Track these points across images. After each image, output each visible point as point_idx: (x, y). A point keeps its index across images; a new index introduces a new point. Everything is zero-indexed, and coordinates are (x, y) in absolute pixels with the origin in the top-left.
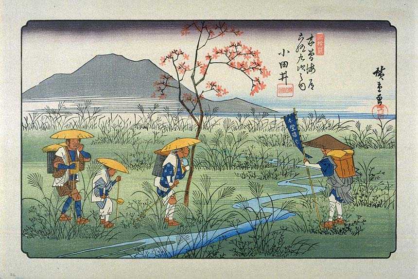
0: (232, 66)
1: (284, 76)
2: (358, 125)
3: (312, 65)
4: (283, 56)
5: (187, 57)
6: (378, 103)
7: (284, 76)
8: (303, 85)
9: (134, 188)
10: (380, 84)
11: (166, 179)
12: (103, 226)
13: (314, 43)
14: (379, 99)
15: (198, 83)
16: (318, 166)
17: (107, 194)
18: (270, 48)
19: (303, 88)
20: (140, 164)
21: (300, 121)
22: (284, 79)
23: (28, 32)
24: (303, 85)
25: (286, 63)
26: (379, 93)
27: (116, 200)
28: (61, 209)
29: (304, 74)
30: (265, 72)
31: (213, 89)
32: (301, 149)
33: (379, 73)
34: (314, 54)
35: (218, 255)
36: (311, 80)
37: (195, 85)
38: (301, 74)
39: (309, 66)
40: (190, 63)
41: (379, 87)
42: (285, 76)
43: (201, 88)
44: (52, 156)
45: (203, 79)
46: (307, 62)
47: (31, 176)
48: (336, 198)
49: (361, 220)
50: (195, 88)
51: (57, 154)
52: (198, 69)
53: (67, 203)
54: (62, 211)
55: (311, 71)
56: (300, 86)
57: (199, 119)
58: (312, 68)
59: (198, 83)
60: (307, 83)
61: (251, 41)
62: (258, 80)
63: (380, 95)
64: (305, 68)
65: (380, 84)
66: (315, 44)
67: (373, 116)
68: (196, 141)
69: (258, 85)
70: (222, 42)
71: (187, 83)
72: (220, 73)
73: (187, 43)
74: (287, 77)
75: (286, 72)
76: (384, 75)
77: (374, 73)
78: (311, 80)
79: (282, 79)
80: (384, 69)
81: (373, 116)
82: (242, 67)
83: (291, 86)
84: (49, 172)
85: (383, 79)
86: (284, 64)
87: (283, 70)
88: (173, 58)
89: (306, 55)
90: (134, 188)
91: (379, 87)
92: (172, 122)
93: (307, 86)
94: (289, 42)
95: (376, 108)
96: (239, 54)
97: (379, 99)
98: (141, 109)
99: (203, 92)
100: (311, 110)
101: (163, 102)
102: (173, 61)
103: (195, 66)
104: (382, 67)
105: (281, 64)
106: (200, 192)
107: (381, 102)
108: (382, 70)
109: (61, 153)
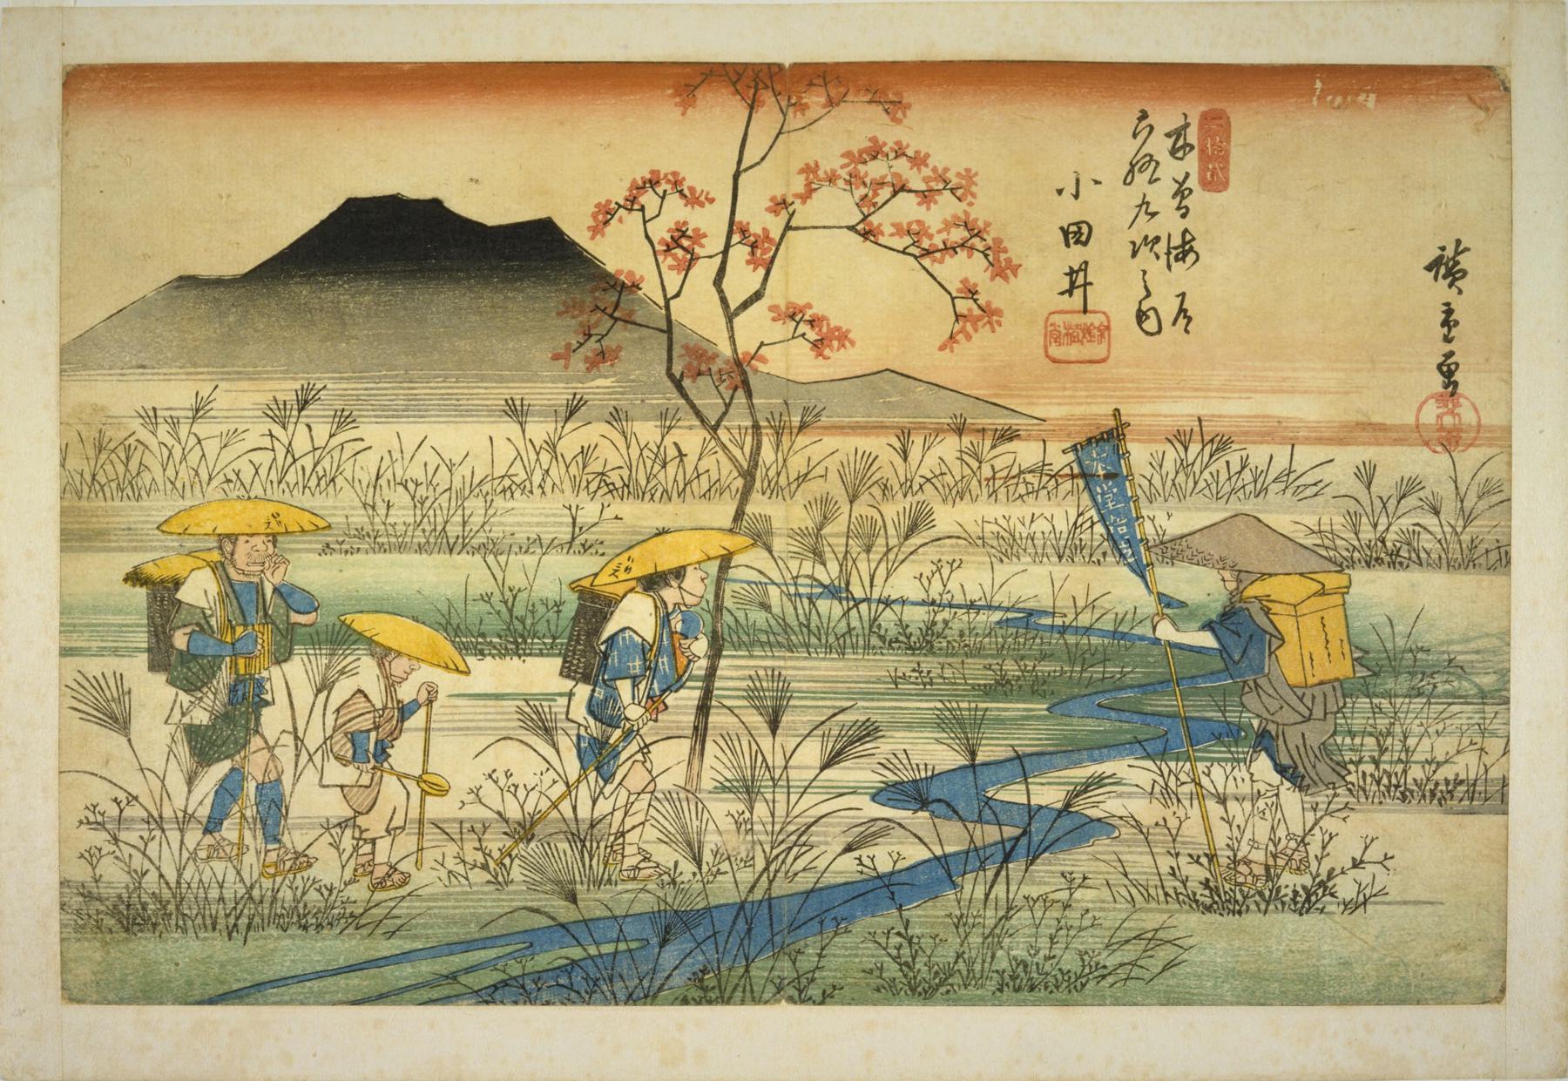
0: (868, 234)
1: (1077, 280)
2: (1366, 475)
3: (1188, 237)
4: (1076, 196)
5: (694, 199)
6: (1446, 387)
7: (1077, 280)
8: (1151, 313)
9: (486, 744)
10: (1449, 312)
11: (613, 696)
12: (365, 881)
13: (1192, 147)
14: (1448, 371)
15: (797, 228)
16: (1207, 640)
17: (382, 753)
18: (1016, 164)
19: (1151, 325)
20: (516, 639)
21: (1139, 454)
22: (1078, 293)
23: (411, 275)
24: (1151, 313)
25: (1085, 229)
26: (1447, 348)
27: (419, 780)
28: (204, 812)
29: (1157, 268)
30: (1003, 269)
31: (803, 335)
32: (1140, 571)
33: (1447, 268)
34: (1191, 191)
35: (815, 992)
36: (1183, 295)
37: (730, 317)
38: (1145, 272)
39: (1176, 241)
40: (710, 222)
41: (1446, 323)
42: (1080, 280)
43: (754, 328)
44: (164, 595)
45: (758, 296)
46: (1169, 225)
47: (87, 685)
48: (1281, 770)
49: (1374, 853)
50: (731, 329)
51: (184, 594)
52: (739, 253)
53: (227, 792)
54: (205, 820)
55: (1183, 259)
56: (1141, 316)
57: (747, 449)
58: (1184, 250)
59: (797, 228)
60: (1168, 309)
61: (943, 134)
62: (972, 293)
63: (1452, 354)
64: (1161, 248)
65: (1449, 312)
66: (1195, 152)
67: (1416, 435)
68: (731, 542)
69: (973, 314)
70: (836, 133)
71: (697, 312)
72: (829, 266)
73: (698, 144)
74: (1086, 284)
75: (1086, 263)
76: (1465, 273)
77: (1428, 268)
78: (1183, 295)
79: (1070, 292)
80: (1467, 249)
81: (1416, 435)
82: (921, 248)
83: (1096, 320)
84: (153, 667)
85: (1460, 292)
86: (1076, 234)
87: (1075, 255)
88: (642, 209)
89: (1162, 197)
90: (486, 744)
91: (1448, 320)
92: (641, 466)
93: (1167, 320)
94: (1097, 141)
95: (1432, 404)
96: (900, 188)
97: (1448, 371)
98: (516, 412)
99: (762, 344)
100: (1095, 409)
101: (601, 385)
102: (645, 222)
103: (729, 238)
104: (1458, 242)
105: (1065, 233)
106: (754, 747)
107: (1456, 384)
108: (1457, 253)
109: (200, 590)
